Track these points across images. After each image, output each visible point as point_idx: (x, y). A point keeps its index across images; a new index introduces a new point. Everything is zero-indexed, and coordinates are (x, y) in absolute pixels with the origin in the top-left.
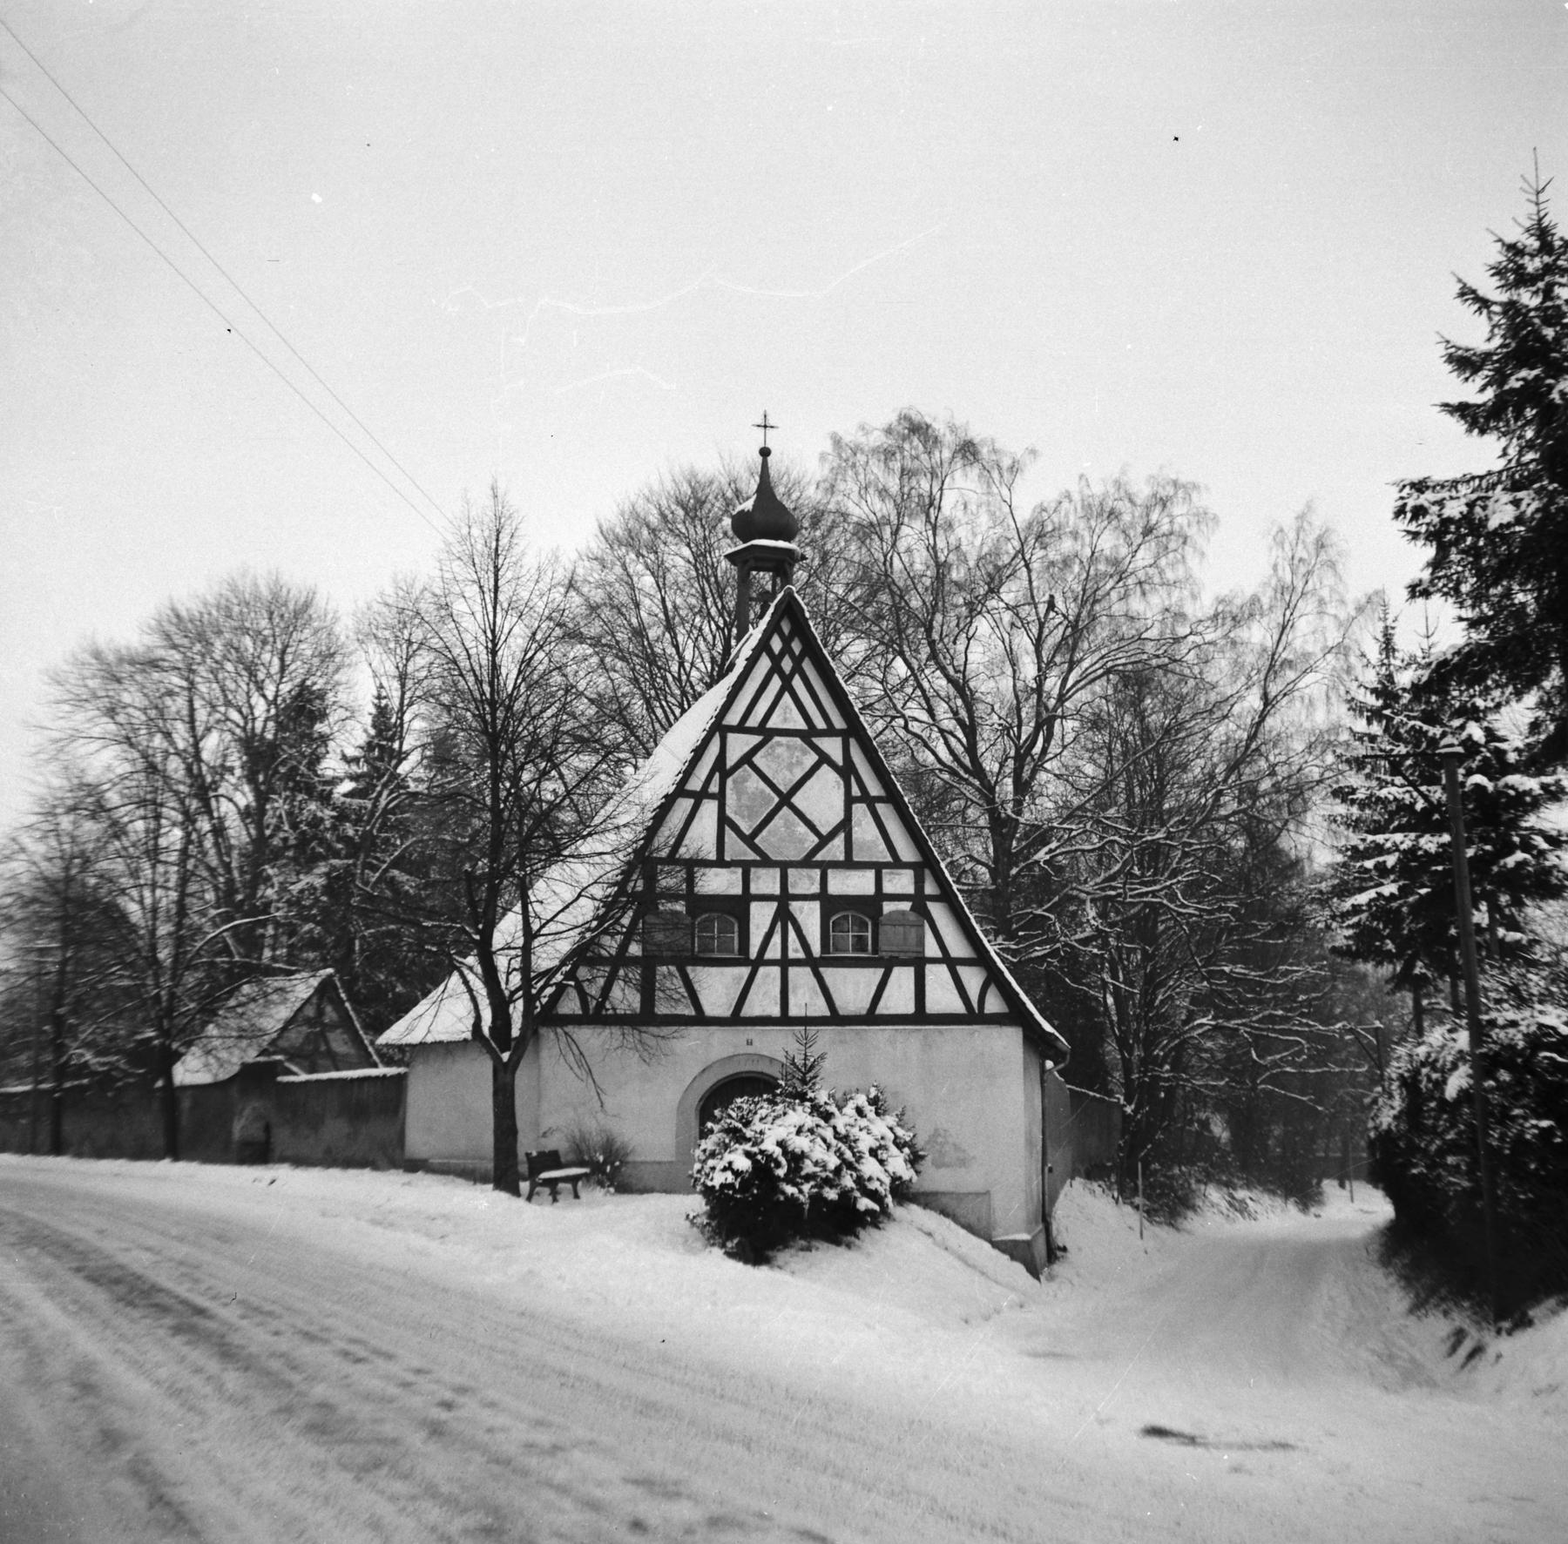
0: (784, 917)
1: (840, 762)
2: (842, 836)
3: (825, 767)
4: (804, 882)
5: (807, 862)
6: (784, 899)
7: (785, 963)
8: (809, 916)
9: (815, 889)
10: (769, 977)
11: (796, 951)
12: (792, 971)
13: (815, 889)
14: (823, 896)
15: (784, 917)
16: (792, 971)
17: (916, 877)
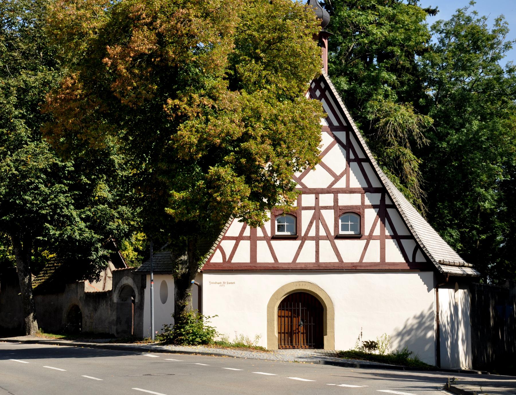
0: (317, 217)
1: (344, 142)
2: (345, 176)
3: (333, 179)
4: (326, 200)
5: (327, 191)
6: (317, 208)
7: (317, 239)
8: (329, 216)
9: (332, 204)
10: (310, 245)
11: (322, 232)
12: (321, 242)
13: (332, 204)
14: (336, 207)
15: (317, 217)
16: (321, 242)
17: (364, 203)
